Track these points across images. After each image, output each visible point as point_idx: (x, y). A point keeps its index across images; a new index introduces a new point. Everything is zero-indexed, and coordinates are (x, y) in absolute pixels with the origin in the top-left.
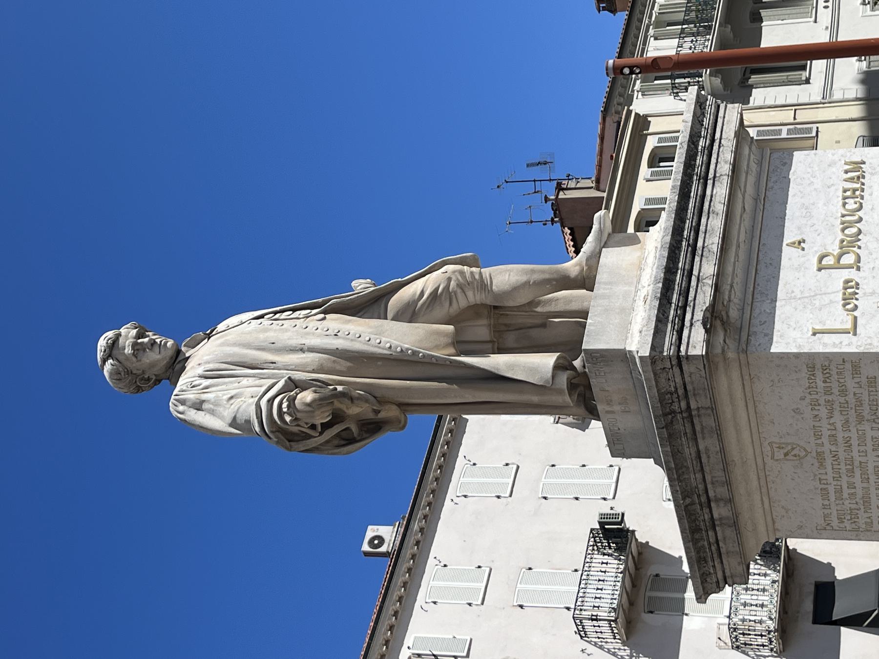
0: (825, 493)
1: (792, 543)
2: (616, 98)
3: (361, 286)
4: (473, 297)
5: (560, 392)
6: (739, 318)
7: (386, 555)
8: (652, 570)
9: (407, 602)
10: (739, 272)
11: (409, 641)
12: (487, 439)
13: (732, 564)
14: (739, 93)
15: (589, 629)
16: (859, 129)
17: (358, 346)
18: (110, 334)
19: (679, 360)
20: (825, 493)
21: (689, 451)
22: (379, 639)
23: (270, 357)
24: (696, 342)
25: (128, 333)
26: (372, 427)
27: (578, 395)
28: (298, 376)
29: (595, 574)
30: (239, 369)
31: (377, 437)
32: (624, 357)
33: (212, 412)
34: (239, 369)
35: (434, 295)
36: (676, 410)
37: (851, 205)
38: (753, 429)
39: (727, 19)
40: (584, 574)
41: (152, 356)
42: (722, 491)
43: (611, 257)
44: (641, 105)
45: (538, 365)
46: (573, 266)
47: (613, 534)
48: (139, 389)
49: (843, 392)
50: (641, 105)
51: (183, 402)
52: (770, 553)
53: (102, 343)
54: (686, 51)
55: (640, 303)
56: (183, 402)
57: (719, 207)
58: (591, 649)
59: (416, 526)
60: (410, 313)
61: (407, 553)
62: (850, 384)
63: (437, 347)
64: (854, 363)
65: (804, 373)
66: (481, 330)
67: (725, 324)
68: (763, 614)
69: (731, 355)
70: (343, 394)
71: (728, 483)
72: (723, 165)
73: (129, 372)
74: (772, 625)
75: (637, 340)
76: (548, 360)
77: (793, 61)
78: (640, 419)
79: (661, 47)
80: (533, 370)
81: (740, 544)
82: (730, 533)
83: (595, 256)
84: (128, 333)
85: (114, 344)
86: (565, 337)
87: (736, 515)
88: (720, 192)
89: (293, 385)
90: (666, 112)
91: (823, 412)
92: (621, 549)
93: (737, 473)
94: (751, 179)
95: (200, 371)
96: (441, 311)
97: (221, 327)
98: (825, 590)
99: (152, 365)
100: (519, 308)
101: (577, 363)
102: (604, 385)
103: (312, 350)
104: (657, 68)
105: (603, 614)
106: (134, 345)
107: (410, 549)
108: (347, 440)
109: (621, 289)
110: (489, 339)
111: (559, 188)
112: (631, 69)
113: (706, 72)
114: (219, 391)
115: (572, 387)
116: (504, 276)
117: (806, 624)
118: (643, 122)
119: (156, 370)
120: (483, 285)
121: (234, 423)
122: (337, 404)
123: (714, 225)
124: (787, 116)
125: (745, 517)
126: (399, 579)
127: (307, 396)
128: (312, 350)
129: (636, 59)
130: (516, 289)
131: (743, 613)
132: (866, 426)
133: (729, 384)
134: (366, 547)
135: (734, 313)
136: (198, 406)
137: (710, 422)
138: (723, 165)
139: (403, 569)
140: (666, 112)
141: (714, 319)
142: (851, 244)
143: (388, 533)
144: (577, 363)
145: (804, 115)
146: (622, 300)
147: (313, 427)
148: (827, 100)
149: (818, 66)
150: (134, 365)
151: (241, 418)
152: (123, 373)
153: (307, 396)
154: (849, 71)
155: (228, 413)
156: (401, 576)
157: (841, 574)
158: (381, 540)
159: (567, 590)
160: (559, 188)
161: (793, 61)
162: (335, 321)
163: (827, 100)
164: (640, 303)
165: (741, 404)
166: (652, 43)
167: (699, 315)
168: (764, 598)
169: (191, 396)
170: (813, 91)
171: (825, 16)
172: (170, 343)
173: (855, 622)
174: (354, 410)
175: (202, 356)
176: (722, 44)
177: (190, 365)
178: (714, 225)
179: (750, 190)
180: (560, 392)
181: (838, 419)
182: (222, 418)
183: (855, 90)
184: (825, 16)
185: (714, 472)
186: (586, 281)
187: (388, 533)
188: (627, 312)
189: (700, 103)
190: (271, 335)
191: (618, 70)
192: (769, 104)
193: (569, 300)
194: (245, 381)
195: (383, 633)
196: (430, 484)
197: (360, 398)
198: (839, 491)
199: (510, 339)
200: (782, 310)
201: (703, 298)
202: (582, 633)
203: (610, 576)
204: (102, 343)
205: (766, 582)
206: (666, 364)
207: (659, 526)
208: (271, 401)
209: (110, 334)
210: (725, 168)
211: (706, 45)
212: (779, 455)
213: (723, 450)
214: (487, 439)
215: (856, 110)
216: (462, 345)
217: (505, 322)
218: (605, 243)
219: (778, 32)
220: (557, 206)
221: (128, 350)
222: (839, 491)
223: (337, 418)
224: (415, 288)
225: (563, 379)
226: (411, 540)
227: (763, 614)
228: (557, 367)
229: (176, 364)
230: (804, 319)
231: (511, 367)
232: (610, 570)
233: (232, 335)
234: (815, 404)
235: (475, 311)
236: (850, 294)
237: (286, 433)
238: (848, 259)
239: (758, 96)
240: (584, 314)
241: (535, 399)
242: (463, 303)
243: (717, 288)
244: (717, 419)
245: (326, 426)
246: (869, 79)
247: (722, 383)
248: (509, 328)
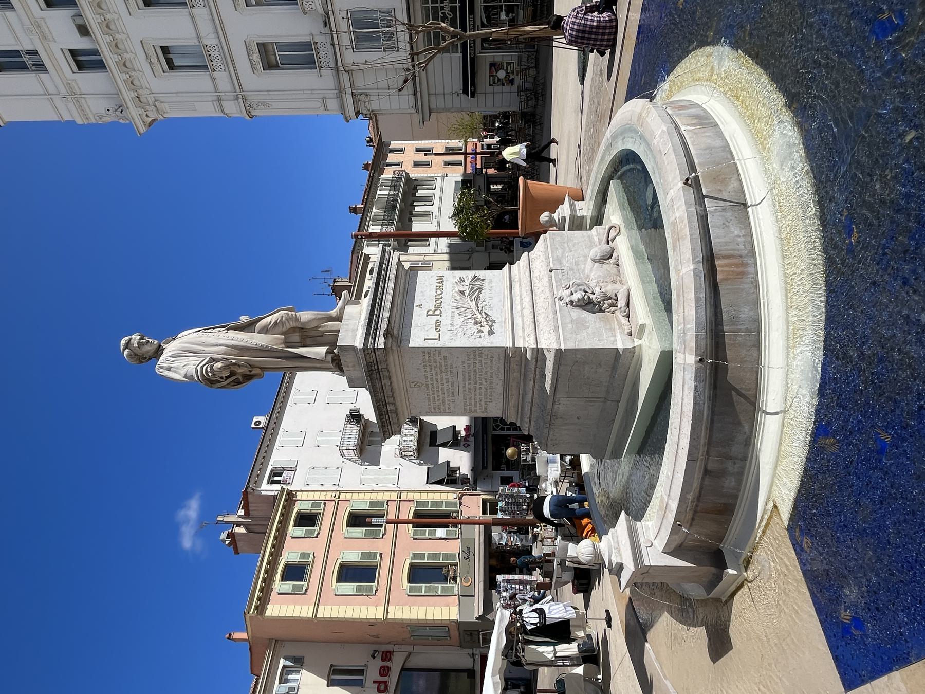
0: (429, 400)
1: (426, 419)
2: (357, 248)
3: (244, 319)
4: (293, 324)
5: (328, 362)
6: (397, 333)
7: (262, 428)
8: (370, 430)
9: (270, 447)
10: (398, 316)
11: (271, 462)
12: (304, 381)
13: (395, 427)
14: (403, 248)
15: (346, 454)
16: (447, 264)
17: (242, 344)
18: (127, 338)
19: (375, 350)
20: (429, 400)
21: (378, 385)
22: (259, 462)
23: (203, 348)
24: (381, 343)
25: (136, 338)
26: (248, 377)
27: (336, 362)
28: (215, 356)
29: (348, 431)
30: (187, 354)
31: (253, 383)
32: (354, 348)
33: (175, 372)
34: (187, 354)
35: (276, 323)
36: (372, 369)
37: (439, 292)
38: (401, 376)
39: (400, 219)
40: (344, 433)
41: (147, 348)
42: (391, 400)
43: (348, 309)
44: (367, 250)
45: (319, 351)
46: (333, 312)
47: (355, 416)
48: (141, 362)
49: (435, 362)
50: (367, 250)
51: (162, 368)
52: (414, 421)
53: (123, 342)
54: (384, 231)
55: (360, 327)
56: (162, 368)
57: (391, 291)
58: (346, 461)
59: (274, 416)
60: (265, 330)
61: (271, 427)
62: (438, 358)
63: (277, 345)
64: (439, 350)
65: (421, 355)
66: (296, 337)
67: (392, 336)
68: (411, 444)
69: (394, 348)
70: (235, 364)
71: (393, 397)
72: (392, 275)
73: (136, 355)
74: (415, 448)
75: (359, 343)
76: (323, 350)
77: (423, 237)
78: (360, 372)
79: (374, 229)
80: (317, 354)
81: (398, 420)
82: (394, 415)
83: (342, 310)
84: (136, 338)
85: (128, 343)
86: (331, 341)
87: (396, 409)
88: (391, 285)
89: (213, 360)
90: (373, 251)
91: (428, 369)
92: (358, 422)
93: (397, 393)
94: (403, 281)
95: (170, 354)
96: (280, 329)
97: (179, 335)
98: (434, 434)
99: (147, 352)
100: (311, 329)
101: (335, 351)
102: (346, 360)
103: (221, 345)
104: (371, 236)
105: (351, 448)
106: (139, 343)
107: (272, 425)
108: (237, 383)
109: (352, 322)
110: (767, 416)
111: (335, 281)
112: (362, 237)
113: (392, 239)
114: (179, 363)
115: (333, 360)
116: (305, 316)
117: (427, 446)
118: (367, 257)
119: (149, 354)
120: (297, 319)
121: (185, 377)
122: (232, 368)
123: (388, 298)
124: (421, 258)
125: (400, 410)
126: (267, 438)
127: (219, 365)
128: (221, 345)
129: (365, 232)
130: (310, 321)
131: (404, 444)
132: (444, 374)
133: (393, 359)
134: (253, 425)
135: (395, 332)
136: (169, 369)
137: (386, 373)
138: (392, 275)
139: (269, 433)
140: (373, 251)
141: (388, 334)
142: (439, 307)
143: (263, 420)
144: (335, 351)
145: (427, 258)
146: (353, 326)
147: (222, 378)
148: (436, 253)
149: (433, 240)
150: (139, 352)
151: (189, 374)
152: (134, 355)
153: (219, 365)
154: (444, 241)
155: (183, 372)
156: (268, 436)
157: (439, 428)
158: (260, 422)
159: (337, 439)
160: (335, 281)
161: (423, 237)
162: (232, 333)
163: (436, 253)
164: (360, 327)
165: (398, 366)
166: (371, 227)
167: (382, 333)
168: (412, 438)
169: (166, 365)
170: (430, 250)
171: (435, 221)
172: (156, 342)
173: (444, 445)
174: (240, 370)
175: (170, 348)
176: (397, 229)
177: (165, 352)
178: (388, 298)
179: (402, 285)
180: (328, 362)
181: (433, 372)
182: (180, 374)
183: (446, 250)
184: (435, 221)
185: (388, 392)
186: (339, 319)
187: (263, 420)
188: (355, 331)
189: (384, 251)
190: (203, 339)
191: (356, 236)
192: (415, 252)
193: (333, 326)
194: (191, 359)
195: (260, 459)
196: (280, 399)
197: (243, 365)
198: (434, 399)
199: (308, 341)
200: (414, 331)
201: (384, 326)
202: (343, 455)
203: (354, 431)
204: (123, 342)
205: (412, 432)
206: (369, 352)
207: (370, 414)
208: (202, 367)
209: (127, 338)
210: (392, 276)
211: (391, 229)
212: (412, 385)
213: (391, 384)
214: (305, 382)
215: (446, 257)
216: (288, 344)
217: (307, 335)
218: (347, 303)
219: (418, 226)
220: (334, 288)
221: (136, 345)
222: (434, 399)
223: (233, 374)
224: (268, 319)
225: (330, 357)
226: (272, 422)
227: (411, 444)
228: (327, 353)
229: (159, 351)
230: (420, 335)
231: (308, 352)
232: (354, 431)
233: (185, 339)
234: (425, 366)
235: (294, 330)
236: (438, 324)
237: (210, 381)
238: (438, 312)
239: (411, 250)
240: (338, 331)
241: (318, 365)
242: (288, 327)
243: (389, 322)
244: (389, 373)
245: (227, 377)
246: (450, 246)
247: (391, 358)
248: (308, 337)
